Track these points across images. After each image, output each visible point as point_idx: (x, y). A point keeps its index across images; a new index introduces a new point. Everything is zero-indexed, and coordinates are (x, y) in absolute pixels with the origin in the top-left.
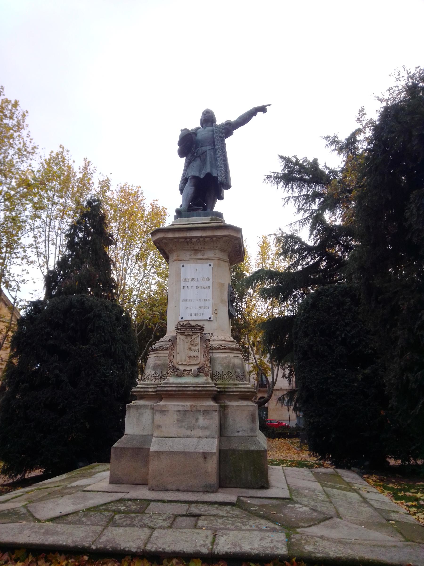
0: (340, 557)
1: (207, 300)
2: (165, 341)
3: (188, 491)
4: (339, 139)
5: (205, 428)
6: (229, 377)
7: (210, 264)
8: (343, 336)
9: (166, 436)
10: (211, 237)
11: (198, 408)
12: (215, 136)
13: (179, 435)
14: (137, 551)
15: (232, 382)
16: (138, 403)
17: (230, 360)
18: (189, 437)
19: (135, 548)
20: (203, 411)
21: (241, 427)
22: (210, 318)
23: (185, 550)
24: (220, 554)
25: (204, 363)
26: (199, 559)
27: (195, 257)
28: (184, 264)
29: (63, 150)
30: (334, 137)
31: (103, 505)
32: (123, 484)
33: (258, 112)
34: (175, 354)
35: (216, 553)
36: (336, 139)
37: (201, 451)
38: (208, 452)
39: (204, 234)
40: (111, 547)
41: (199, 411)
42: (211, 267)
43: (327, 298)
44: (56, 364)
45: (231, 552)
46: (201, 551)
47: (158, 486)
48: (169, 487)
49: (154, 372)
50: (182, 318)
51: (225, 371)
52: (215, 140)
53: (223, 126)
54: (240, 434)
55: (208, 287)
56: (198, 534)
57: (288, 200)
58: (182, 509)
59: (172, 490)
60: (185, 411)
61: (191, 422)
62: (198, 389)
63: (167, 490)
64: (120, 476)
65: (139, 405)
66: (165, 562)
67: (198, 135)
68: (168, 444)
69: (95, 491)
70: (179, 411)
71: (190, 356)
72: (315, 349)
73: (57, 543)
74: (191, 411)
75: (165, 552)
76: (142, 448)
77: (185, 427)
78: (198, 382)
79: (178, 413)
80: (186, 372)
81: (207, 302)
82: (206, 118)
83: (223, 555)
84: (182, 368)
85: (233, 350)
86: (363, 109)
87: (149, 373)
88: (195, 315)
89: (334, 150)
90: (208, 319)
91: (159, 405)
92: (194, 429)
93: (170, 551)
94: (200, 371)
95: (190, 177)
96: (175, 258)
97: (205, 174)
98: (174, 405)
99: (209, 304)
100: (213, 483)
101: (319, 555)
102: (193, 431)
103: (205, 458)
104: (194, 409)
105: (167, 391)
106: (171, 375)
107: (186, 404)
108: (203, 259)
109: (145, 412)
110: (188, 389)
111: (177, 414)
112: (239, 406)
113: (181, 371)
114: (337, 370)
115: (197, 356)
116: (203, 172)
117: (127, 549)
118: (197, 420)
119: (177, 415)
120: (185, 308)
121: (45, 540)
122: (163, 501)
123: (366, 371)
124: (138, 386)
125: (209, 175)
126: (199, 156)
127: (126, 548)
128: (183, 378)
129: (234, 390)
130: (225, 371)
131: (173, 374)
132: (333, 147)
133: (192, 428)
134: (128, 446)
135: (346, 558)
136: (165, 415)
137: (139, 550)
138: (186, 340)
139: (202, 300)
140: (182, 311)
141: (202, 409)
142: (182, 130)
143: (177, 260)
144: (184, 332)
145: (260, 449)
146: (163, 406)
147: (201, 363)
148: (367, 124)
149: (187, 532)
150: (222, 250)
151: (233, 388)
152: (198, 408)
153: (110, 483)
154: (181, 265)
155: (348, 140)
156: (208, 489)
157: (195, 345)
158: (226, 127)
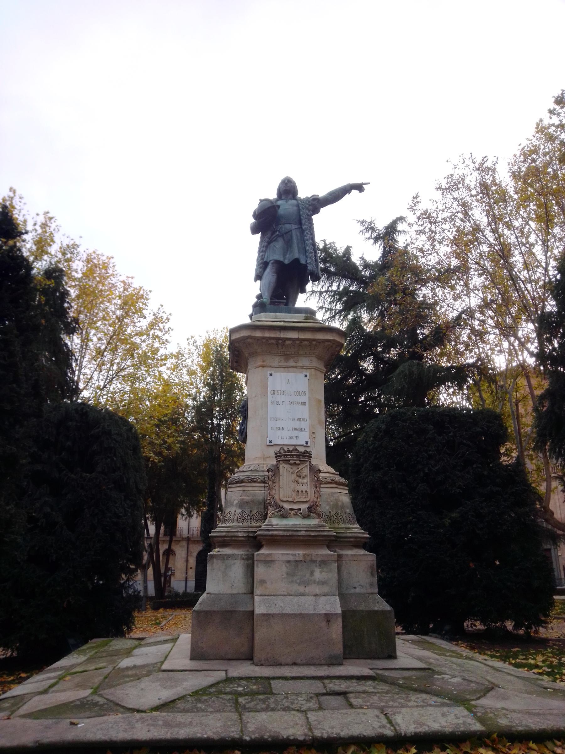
0: (544, 729)
1: (303, 420)
2: (252, 471)
3: (307, 664)
4: (376, 226)
5: (323, 583)
6: (338, 520)
7: (306, 374)
8: (426, 470)
9: (272, 594)
10: (278, 339)
11: (313, 557)
12: (301, 213)
13: (290, 592)
14: (304, 740)
15: (343, 526)
16: (222, 551)
17: (338, 497)
18: (303, 595)
19: (302, 735)
20: (320, 561)
21: (359, 582)
22: (307, 443)
23: (365, 734)
24: (407, 735)
25: (315, 500)
26: (382, 744)
27: (285, 364)
28: (272, 372)
29: (15, 196)
30: (371, 223)
31: (212, 686)
32: (210, 659)
33: (353, 191)
34: (276, 488)
35: (403, 734)
36: (373, 225)
37: (323, 612)
38: (332, 614)
39: (302, 336)
40: (270, 737)
41: (315, 562)
42: (306, 379)
43: (404, 424)
44: (47, 499)
45: (420, 732)
46: (385, 733)
47: (267, 660)
48: (283, 660)
49: (240, 511)
50: (270, 442)
51: (333, 511)
52: (302, 217)
53: (309, 202)
54: (358, 590)
55: (304, 404)
56: (364, 714)
57: (310, 295)
58: (318, 687)
59: (287, 665)
60: (297, 561)
61: (305, 576)
62: (313, 534)
63: (280, 665)
64: (205, 649)
65: (226, 555)
66: (340, 750)
67: (280, 208)
68: (278, 605)
69: (179, 671)
70: (289, 562)
71: (298, 491)
72: (390, 487)
73: (194, 736)
74: (305, 562)
75: (341, 738)
76: (235, 611)
77: (297, 583)
78: (309, 525)
79: (288, 565)
80: (293, 512)
81: (303, 422)
82: (288, 188)
83: (412, 736)
84: (287, 506)
85: (339, 485)
86: (416, 197)
87: (233, 512)
88: (287, 438)
89: (369, 238)
90: (305, 444)
91: (262, 554)
92: (308, 584)
93: (346, 736)
94: (312, 510)
95: (272, 262)
96: (260, 363)
97: (291, 260)
98: (283, 554)
99: (305, 425)
100: (339, 652)
101: (520, 728)
102: (307, 588)
103: (328, 621)
104: (309, 558)
105: (272, 536)
106: (274, 516)
107: (298, 552)
108: (296, 367)
109: (234, 564)
110: (299, 533)
111: (286, 566)
112: (355, 555)
113: (287, 510)
114: (419, 512)
115: (306, 491)
116: (287, 256)
117: (292, 738)
118: (312, 573)
119: (287, 567)
120: (275, 428)
121: (174, 734)
122: (286, 678)
123: (454, 515)
124: (217, 530)
125: (296, 261)
126: (282, 236)
127: (289, 736)
128: (289, 519)
129: (348, 535)
130: (333, 511)
131: (276, 514)
132: (368, 235)
133: (306, 583)
134: (215, 609)
135: (551, 730)
136: (270, 567)
137: (307, 738)
138: (291, 470)
139: (296, 419)
140: (270, 432)
141: (319, 559)
142: (261, 201)
143: (263, 366)
144: (289, 460)
145: (386, 609)
146: (268, 555)
147: (312, 500)
148: (422, 214)
149: (349, 713)
150: (319, 358)
151: (346, 533)
152: (314, 558)
153: (191, 659)
154: (269, 373)
155: (387, 228)
156: (333, 661)
157: (303, 477)
158: (314, 203)
